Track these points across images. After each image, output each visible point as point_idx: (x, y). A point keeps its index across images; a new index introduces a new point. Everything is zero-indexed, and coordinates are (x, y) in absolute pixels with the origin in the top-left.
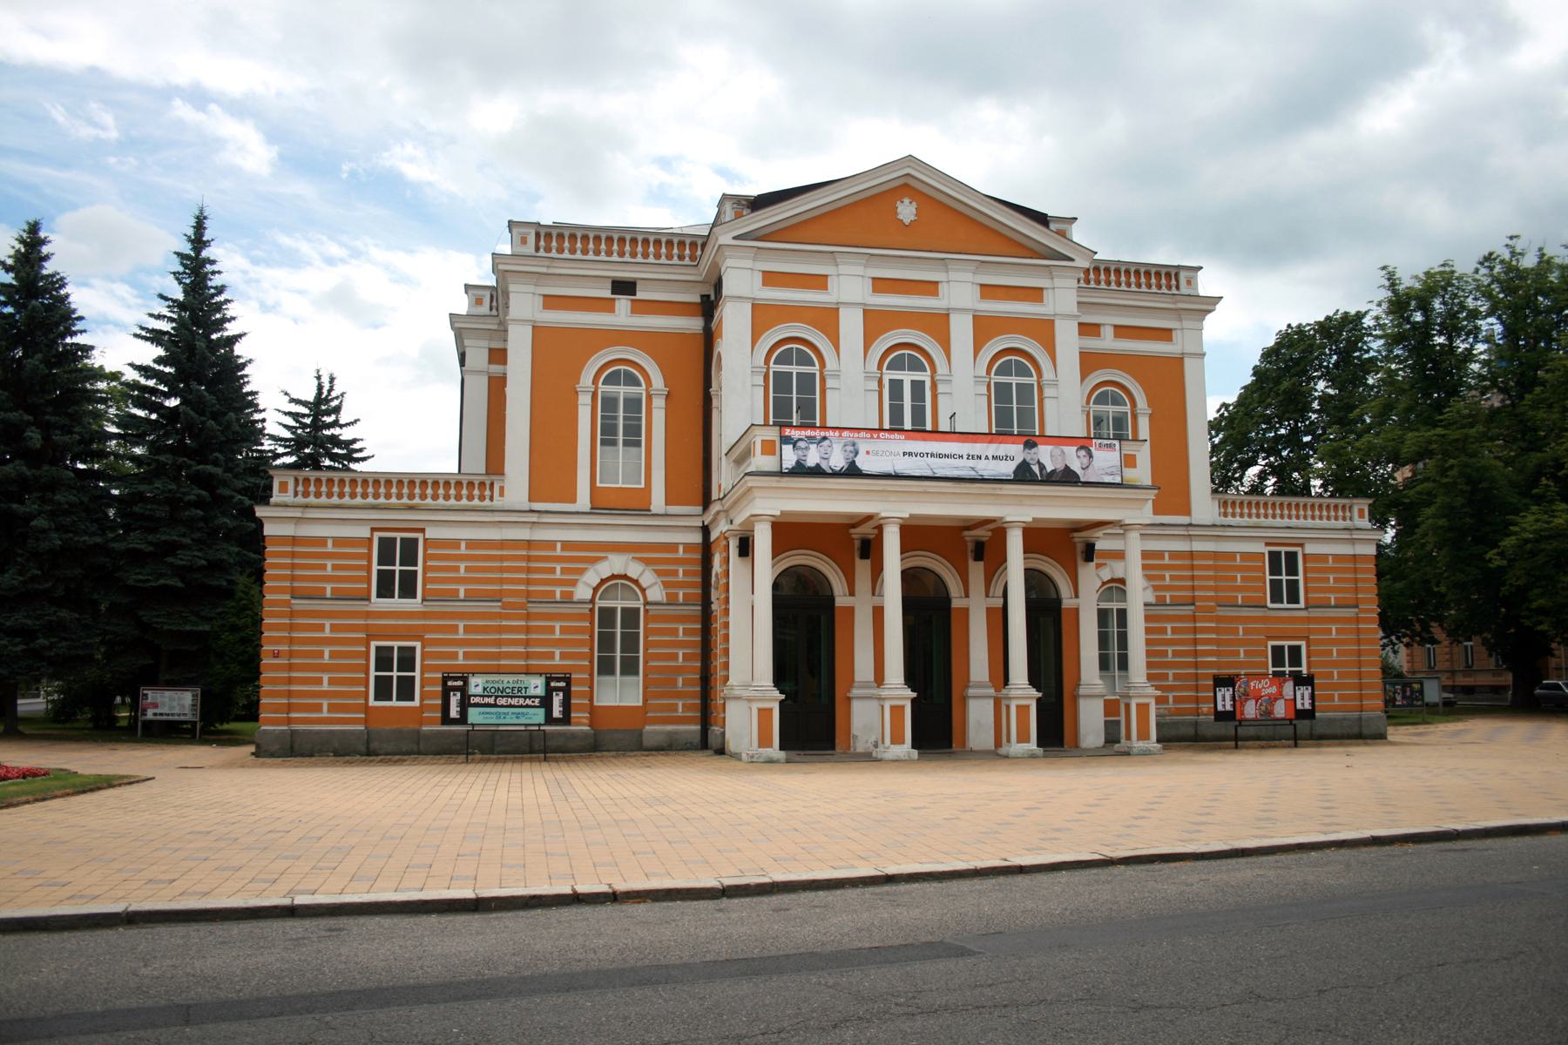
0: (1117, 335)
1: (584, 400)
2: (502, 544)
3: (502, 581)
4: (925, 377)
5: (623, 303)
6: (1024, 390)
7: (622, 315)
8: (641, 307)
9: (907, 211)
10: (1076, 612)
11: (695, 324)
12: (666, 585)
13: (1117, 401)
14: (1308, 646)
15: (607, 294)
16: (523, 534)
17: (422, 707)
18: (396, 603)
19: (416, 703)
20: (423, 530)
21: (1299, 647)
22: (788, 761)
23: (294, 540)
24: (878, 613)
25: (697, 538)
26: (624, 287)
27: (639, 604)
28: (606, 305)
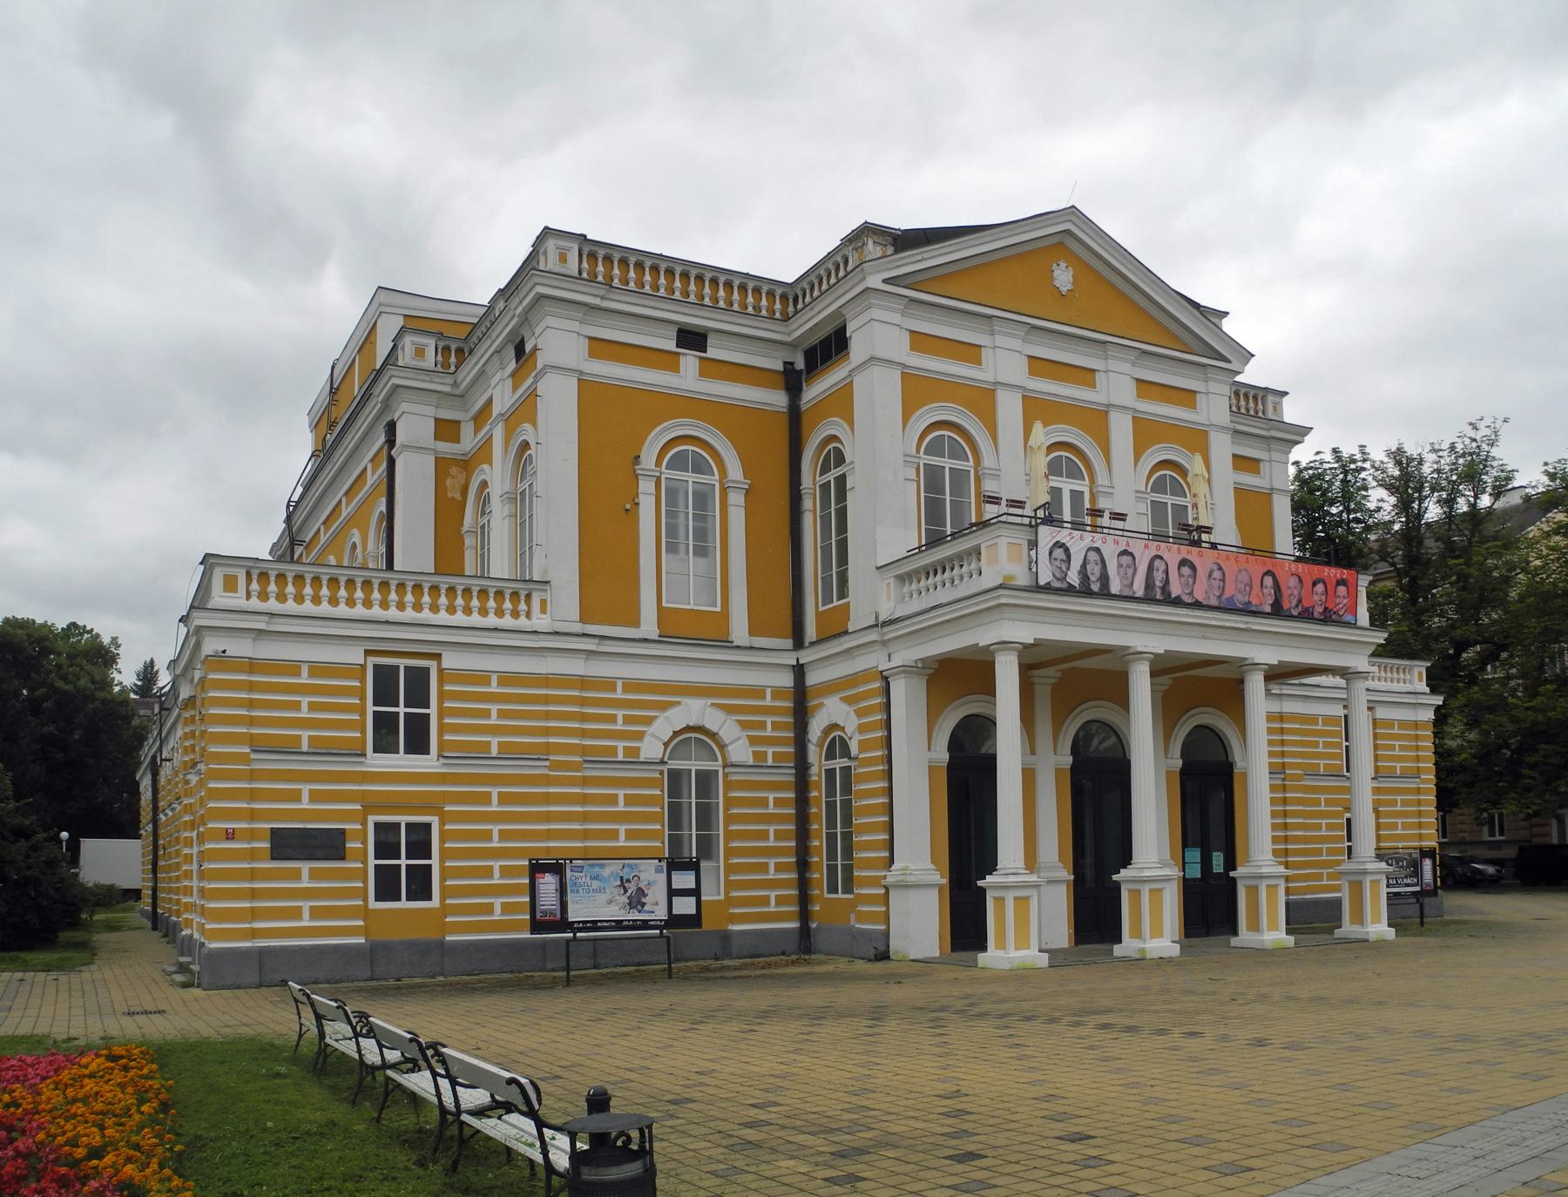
0: (703, 373)
1: (646, 486)
2: (547, 680)
3: (548, 732)
4: (1083, 486)
5: (689, 360)
7: (688, 376)
8: (714, 369)
9: (1063, 277)
11: (777, 399)
12: (753, 741)
13: (700, 467)
14: (442, 823)
15: (671, 345)
16: (576, 667)
17: (445, 910)
18: (401, 762)
20: (438, 657)
21: (428, 826)
23: (252, 665)
25: (787, 680)
26: (692, 339)
27: (717, 765)
28: (668, 361)
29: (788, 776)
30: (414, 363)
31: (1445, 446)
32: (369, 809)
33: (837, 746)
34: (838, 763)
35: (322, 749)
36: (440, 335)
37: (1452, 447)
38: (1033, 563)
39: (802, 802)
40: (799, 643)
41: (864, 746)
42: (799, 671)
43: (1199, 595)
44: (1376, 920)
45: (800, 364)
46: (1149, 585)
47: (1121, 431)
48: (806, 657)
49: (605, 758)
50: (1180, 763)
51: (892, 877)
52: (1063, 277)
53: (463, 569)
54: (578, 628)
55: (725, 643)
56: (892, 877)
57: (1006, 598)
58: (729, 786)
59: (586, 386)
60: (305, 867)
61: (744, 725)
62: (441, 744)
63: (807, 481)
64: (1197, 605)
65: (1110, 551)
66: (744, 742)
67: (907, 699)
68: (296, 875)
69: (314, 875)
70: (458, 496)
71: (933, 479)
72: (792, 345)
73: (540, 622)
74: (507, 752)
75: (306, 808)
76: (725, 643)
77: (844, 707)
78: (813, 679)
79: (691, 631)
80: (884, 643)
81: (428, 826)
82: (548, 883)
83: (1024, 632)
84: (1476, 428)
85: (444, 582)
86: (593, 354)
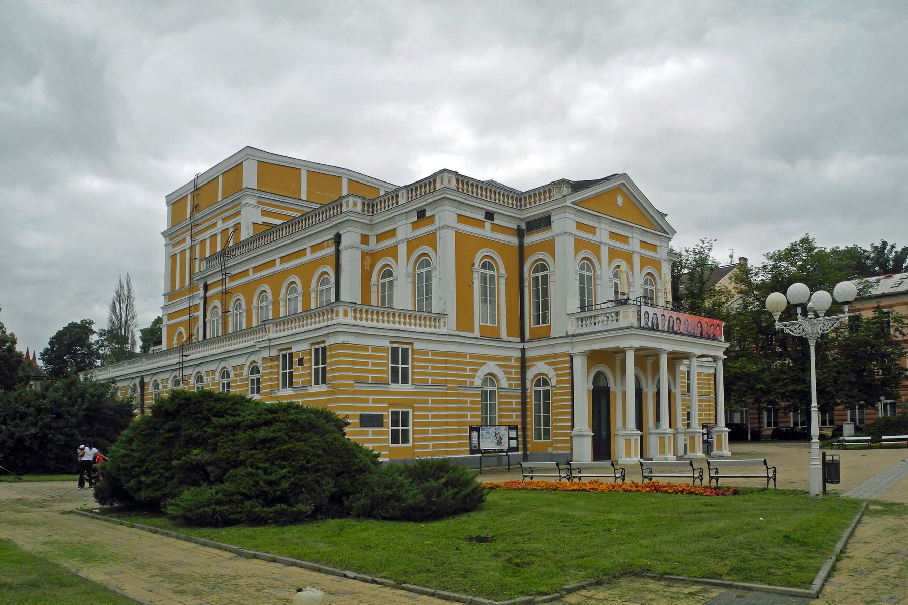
0: (492, 230)
1: (476, 276)
2: (446, 354)
3: (447, 375)
5: (488, 224)
6: (589, 277)
7: (487, 232)
8: (497, 228)
9: (620, 200)
10: (646, 394)
11: (514, 241)
12: (509, 379)
15: (483, 218)
17: (414, 447)
18: (399, 387)
19: (410, 444)
20: (411, 344)
21: (408, 413)
22: (104, 512)
24: (624, 394)
25: (518, 354)
29: (518, 393)
30: (353, 210)
31: (691, 249)
32: (391, 406)
33: (542, 381)
34: (255, 376)
35: (377, 382)
36: (363, 198)
37: (694, 251)
38: (639, 319)
39: (524, 403)
40: (523, 340)
41: (558, 382)
42: (523, 351)
43: (682, 330)
44: (670, 453)
45: (523, 227)
46: (669, 327)
47: (636, 260)
48: (526, 346)
49: (462, 385)
50: (592, 387)
51: (573, 433)
52: (620, 200)
53: (370, 301)
54: (456, 333)
55: (499, 339)
56: (573, 433)
57: (633, 331)
58: (500, 397)
59: (459, 236)
60: (370, 429)
61: (506, 372)
62: (413, 380)
63: (526, 275)
64: (681, 334)
65: (659, 315)
66: (505, 379)
67: (579, 365)
68: (367, 433)
69: (374, 433)
70: (368, 268)
71: (582, 277)
72: (521, 220)
73: (444, 330)
74: (435, 383)
75: (371, 407)
76: (499, 339)
77: (548, 367)
78: (528, 354)
79: (490, 335)
80: (571, 343)
81: (408, 413)
82: (475, 434)
83: (636, 344)
84: (703, 242)
85: (365, 307)
86: (459, 221)
